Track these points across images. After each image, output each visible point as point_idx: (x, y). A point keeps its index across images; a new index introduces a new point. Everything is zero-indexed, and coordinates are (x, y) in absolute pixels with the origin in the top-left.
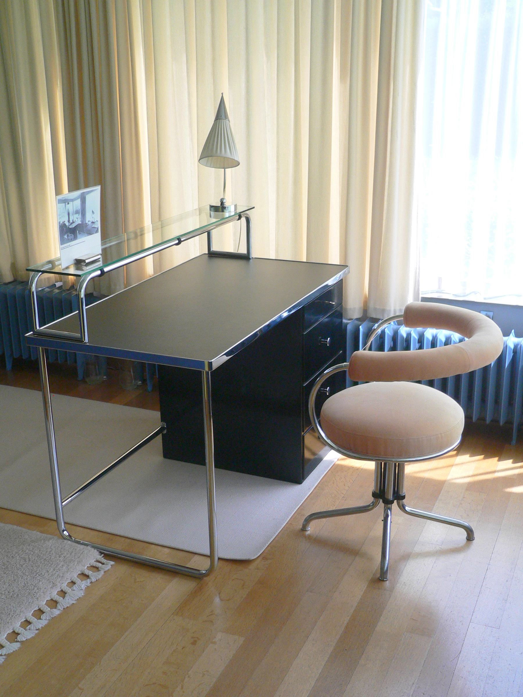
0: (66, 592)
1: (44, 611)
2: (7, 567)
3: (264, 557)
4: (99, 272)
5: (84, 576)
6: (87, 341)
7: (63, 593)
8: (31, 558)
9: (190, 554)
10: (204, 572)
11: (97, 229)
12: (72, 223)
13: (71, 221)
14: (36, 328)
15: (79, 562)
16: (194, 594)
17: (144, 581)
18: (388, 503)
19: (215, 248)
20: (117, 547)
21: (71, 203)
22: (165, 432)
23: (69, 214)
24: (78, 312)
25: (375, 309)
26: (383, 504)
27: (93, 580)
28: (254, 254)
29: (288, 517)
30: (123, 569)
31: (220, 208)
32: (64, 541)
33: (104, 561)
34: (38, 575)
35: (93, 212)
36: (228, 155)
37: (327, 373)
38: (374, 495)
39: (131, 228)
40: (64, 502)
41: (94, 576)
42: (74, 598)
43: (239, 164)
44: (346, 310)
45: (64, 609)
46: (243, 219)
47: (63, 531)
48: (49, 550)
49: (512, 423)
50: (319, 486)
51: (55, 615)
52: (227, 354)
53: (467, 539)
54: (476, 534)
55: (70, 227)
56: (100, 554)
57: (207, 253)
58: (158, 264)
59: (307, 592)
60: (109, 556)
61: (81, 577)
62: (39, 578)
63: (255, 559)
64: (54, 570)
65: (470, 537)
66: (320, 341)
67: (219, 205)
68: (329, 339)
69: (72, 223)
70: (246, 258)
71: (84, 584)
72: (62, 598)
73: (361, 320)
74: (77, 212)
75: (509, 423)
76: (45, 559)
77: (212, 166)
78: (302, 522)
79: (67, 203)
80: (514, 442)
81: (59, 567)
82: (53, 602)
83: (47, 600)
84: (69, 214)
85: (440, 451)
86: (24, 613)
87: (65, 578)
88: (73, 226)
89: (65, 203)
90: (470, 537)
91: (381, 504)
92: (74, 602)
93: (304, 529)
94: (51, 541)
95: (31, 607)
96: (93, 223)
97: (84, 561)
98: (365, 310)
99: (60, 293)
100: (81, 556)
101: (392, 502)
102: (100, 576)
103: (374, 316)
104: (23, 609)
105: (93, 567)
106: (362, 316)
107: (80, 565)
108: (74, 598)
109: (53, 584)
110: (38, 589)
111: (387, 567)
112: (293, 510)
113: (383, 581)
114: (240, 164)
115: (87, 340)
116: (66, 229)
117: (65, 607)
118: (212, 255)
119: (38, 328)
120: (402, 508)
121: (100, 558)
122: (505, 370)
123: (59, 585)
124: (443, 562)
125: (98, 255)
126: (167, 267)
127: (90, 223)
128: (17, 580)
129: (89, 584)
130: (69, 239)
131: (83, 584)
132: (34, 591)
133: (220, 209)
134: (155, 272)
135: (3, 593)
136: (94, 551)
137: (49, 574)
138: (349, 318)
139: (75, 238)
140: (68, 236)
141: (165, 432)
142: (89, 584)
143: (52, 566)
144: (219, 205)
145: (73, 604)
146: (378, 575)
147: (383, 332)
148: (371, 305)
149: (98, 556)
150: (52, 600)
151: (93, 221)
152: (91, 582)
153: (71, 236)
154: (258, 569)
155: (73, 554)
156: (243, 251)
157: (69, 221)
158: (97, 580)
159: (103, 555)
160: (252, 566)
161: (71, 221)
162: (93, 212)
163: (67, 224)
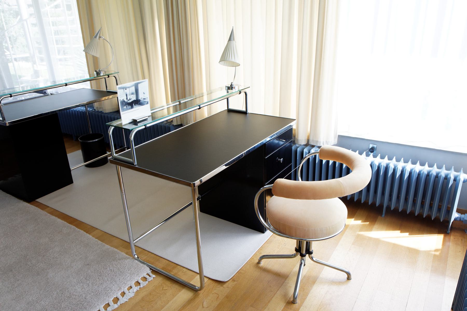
0: (125, 293)
1: (110, 305)
2: (101, 275)
3: (233, 279)
4: (144, 127)
5: (138, 283)
6: (136, 164)
7: (123, 294)
8: (114, 270)
9: (195, 273)
10: (197, 288)
11: (147, 102)
12: (129, 100)
13: (128, 99)
14: (114, 155)
15: (137, 275)
16: (190, 301)
17: (167, 289)
18: (302, 256)
19: (231, 107)
20: (159, 266)
21: (128, 89)
22: (200, 199)
23: (127, 95)
24: (130, 149)
25: (313, 140)
26: (300, 257)
27: (142, 286)
28: (249, 111)
29: (252, 254)
30: (160, 280)
31: (230, 88)
32: (134, 261)
33: (151, 274)
34: (114, 281)
35: (144, 93)
36: (233, 60)
37: (266, 187)
38: (296, 250)
39: (197, 93)
40: (135, 240)
41: (143, 284)
42: (128, 297)
43: (240, 65)
44: (298, 140)
45: (121, 304)
46: (243, 94)
47: (135, 255)
48: (125, 266)
49: (383, 206)
50: (252, 258)
51: (114, 308)
52: (226, 165)
53: (347, 278)
54: (352, 276)
55: (128, 102)
56: (150, 270)
57: (227, 109)
58: (209, 111)
59: (250, 307)
60: (155, 271)
61: (137, 283)
62: (114, 283)
63: (227, 281)
64: (123, 279)
65: (349, 278)
66: (278, 160)
67: (230, 86)
68: (282, 159)
69: (129, 100)
70: (245, 113)
71: (135, 289)
72: (122, 297)
73: (306, 145)
74: (132, 94)
75: (381, 206)
76: (121, 271)
77: (227, 65)
78: (258, 258)
79: (125, 89)
80: (383, 215)
81: (126, 277)
82: (117, 299)
83: (114, 298)
84: (127, 95)
85: (329, 236)
86: (99, 306)
87: (127, 284)
88: (130, 101)
89: (124, 89)
90: (349, 278)
91: (299, 257)
92: (127, 300)
93: (259, 263)
94: (128, 260)
95: (104, 302)
96: (144, 99)
97: (140, 274)
98: (308, 141)
99: (166, 123)
100: (139, 271)
101: (305, 256)
102: (145, 285)
103: (312, 144)
104: (100, 303)
105: (144, 277)
106: (305, 144)
107: (138, 277)
108: (128, 297)
109: (120, 288)
110: (111, 291)
111: (297, 296)
112: (256, 250)
113: (294, 303)
114: (241, 65)
115: (136, 163)
116: (125, 103)
117: (122, 303)
118: (230, 111)
119: (114, 155)
120: (312, 258)
121: (149, 272)
122: (381, 176)
123: (122, 288)
124: (334, 288)
125: (147, 117)
126: (214, 113)
127: (142, 99)
128: (103, 284)
129: (138, 289)
130: (127, 109)
131: (135, 288)
132: (108, 292)
133: (231, 88)
134: (208, 115)
135: (93, 291)
136: (147, 268)
137: (120, 281)
138: (299, 144)
139: (132, 107)
140: (126, 107)
141: (200, 199)
142: (138, 289)
143: (123, 276)
144: (230, 86)
145: (126, 301)
146: (292, 299)
147: (309, 159)
148: (311, 139)
149: (149, 271)
150: (117, 297)
151: (144, 98)
152: (140, 288)
153: (129, 107)
154: (228, 288)
155: (136, 269)
156: (244, 109)
157: (127, 99)
158: (143, 287)
159: (151, 270)
160: (225, 286)
161: (128, 99)
162: (144, 93)
163: (126, 100)
